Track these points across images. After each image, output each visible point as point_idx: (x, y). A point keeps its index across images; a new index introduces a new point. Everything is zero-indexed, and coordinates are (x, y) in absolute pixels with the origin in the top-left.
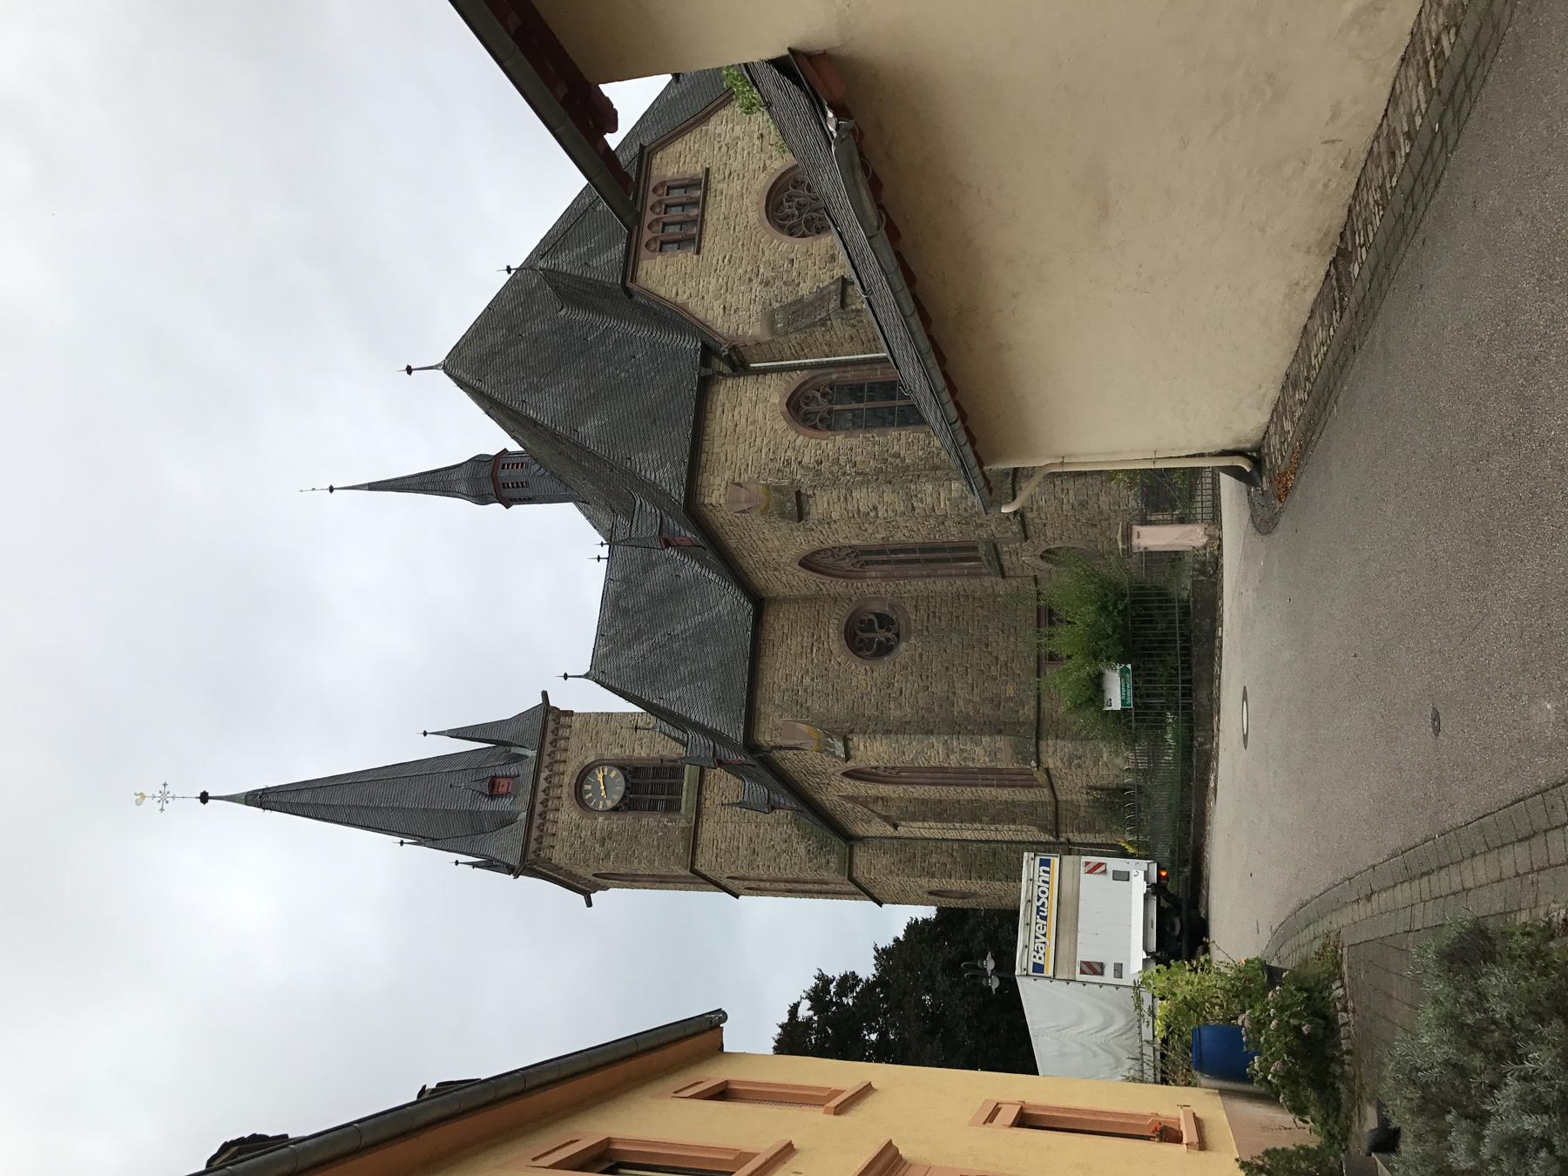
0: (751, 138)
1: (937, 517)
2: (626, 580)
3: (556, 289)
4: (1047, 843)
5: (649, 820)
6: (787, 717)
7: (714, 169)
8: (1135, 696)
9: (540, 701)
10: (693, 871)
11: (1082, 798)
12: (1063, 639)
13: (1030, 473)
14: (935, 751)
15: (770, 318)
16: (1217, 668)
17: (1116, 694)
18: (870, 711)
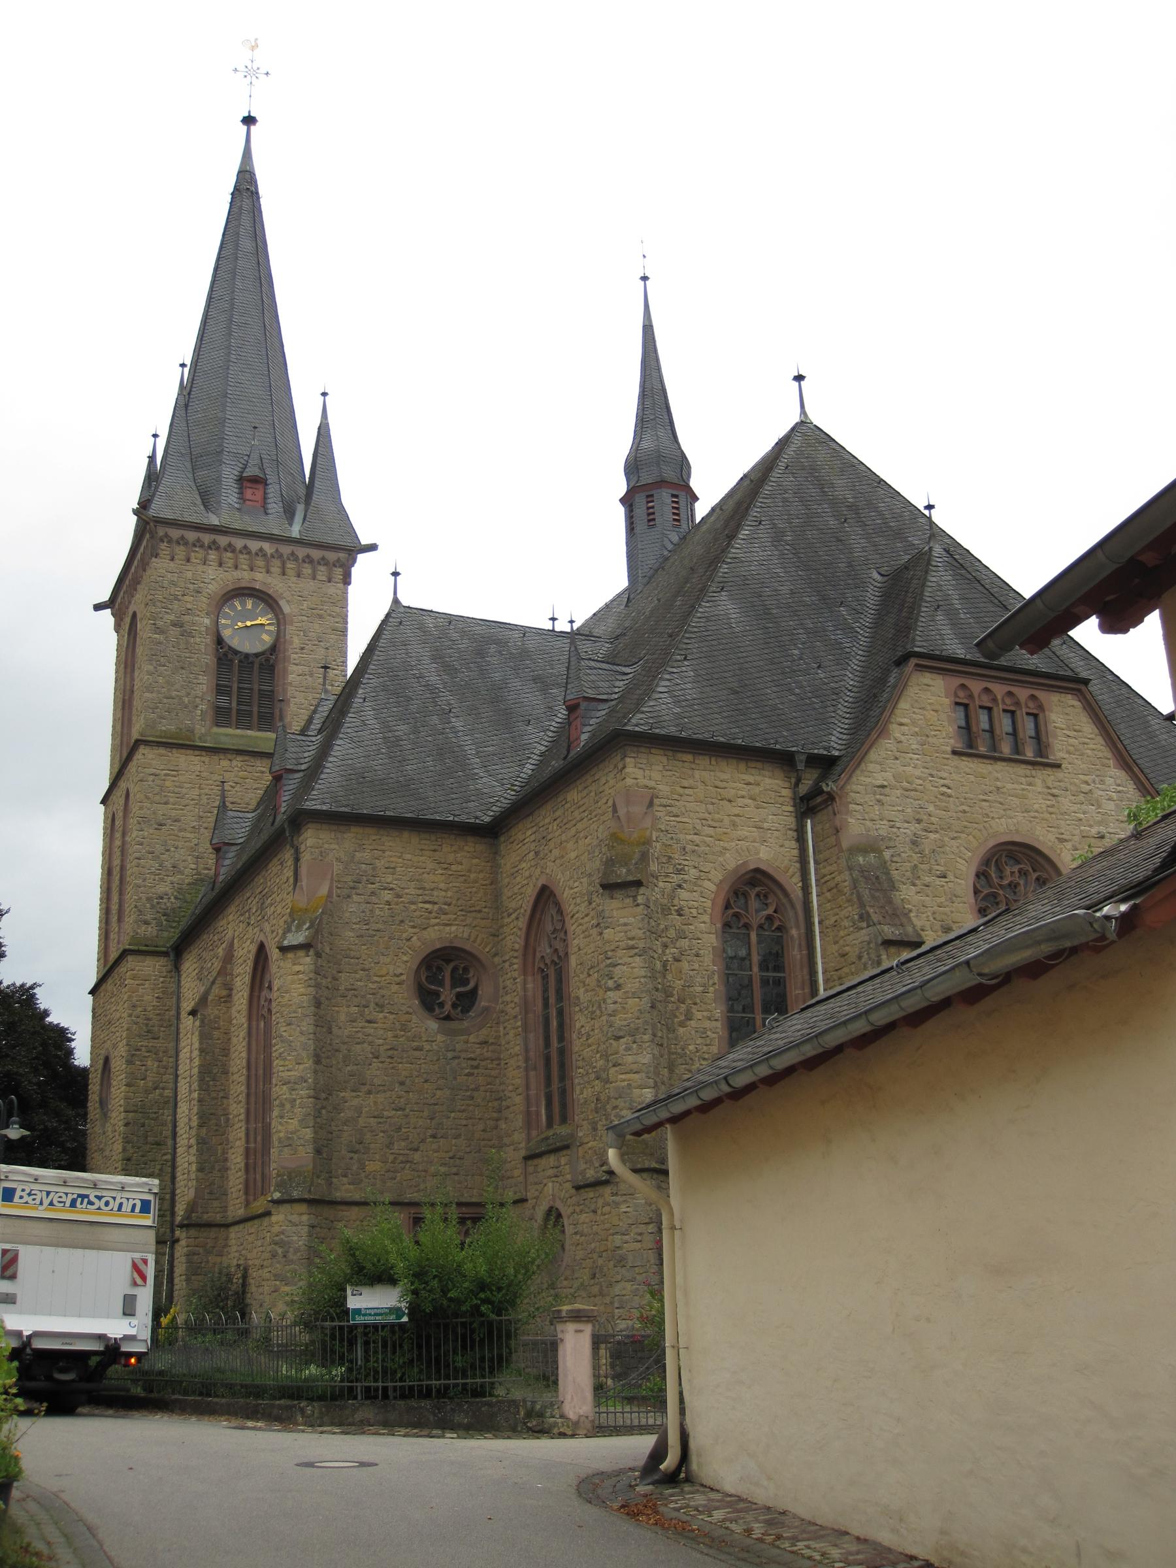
0: (1100, 823)
1: (606, 1070)
2: (524, 653)
3: (906, 568)
4: (173, 1214)
5: (204, 685)
6: (337, 868)
7: (1060, 774)
8: (366, 1326)
9: (364, 540)
10: (138, 743)
11: (231, 1260)
12: (441, 1235)
13: (663, 1188)
14: (292, 1066)
15: (870, 847)
16: (403, 1431)
17: (370, 1302)
18: (345, 980)
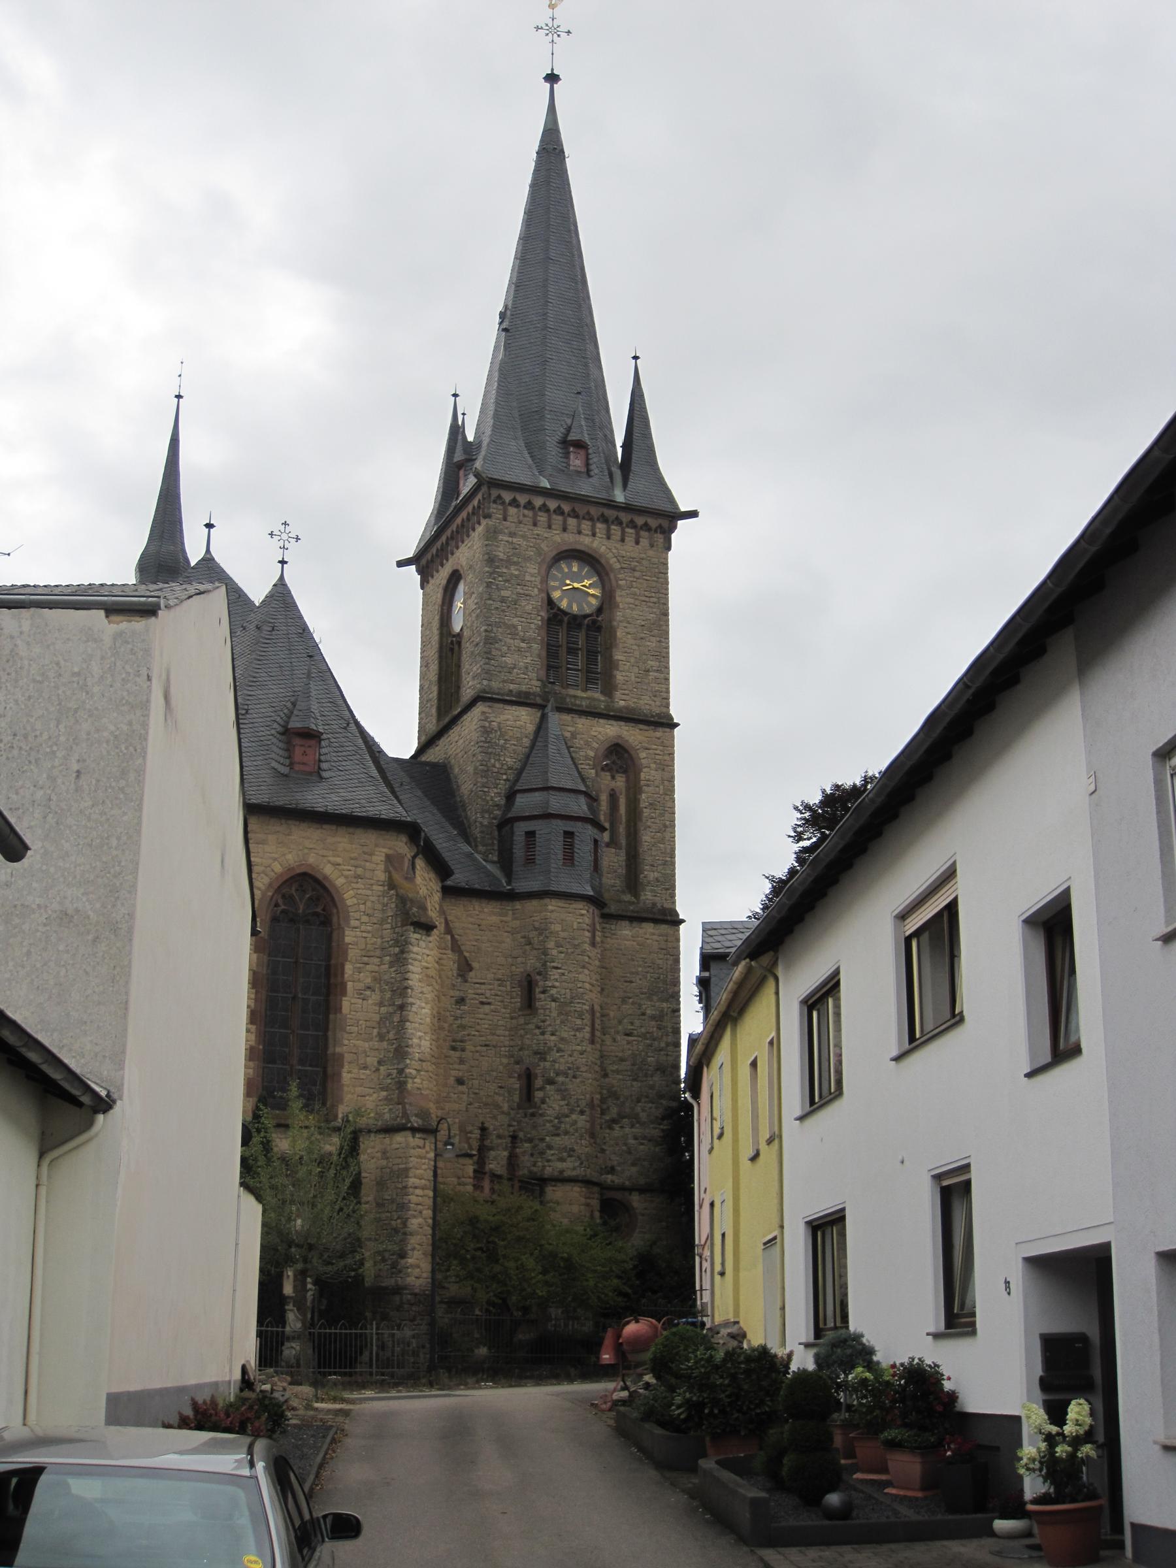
9: (683, 508)
